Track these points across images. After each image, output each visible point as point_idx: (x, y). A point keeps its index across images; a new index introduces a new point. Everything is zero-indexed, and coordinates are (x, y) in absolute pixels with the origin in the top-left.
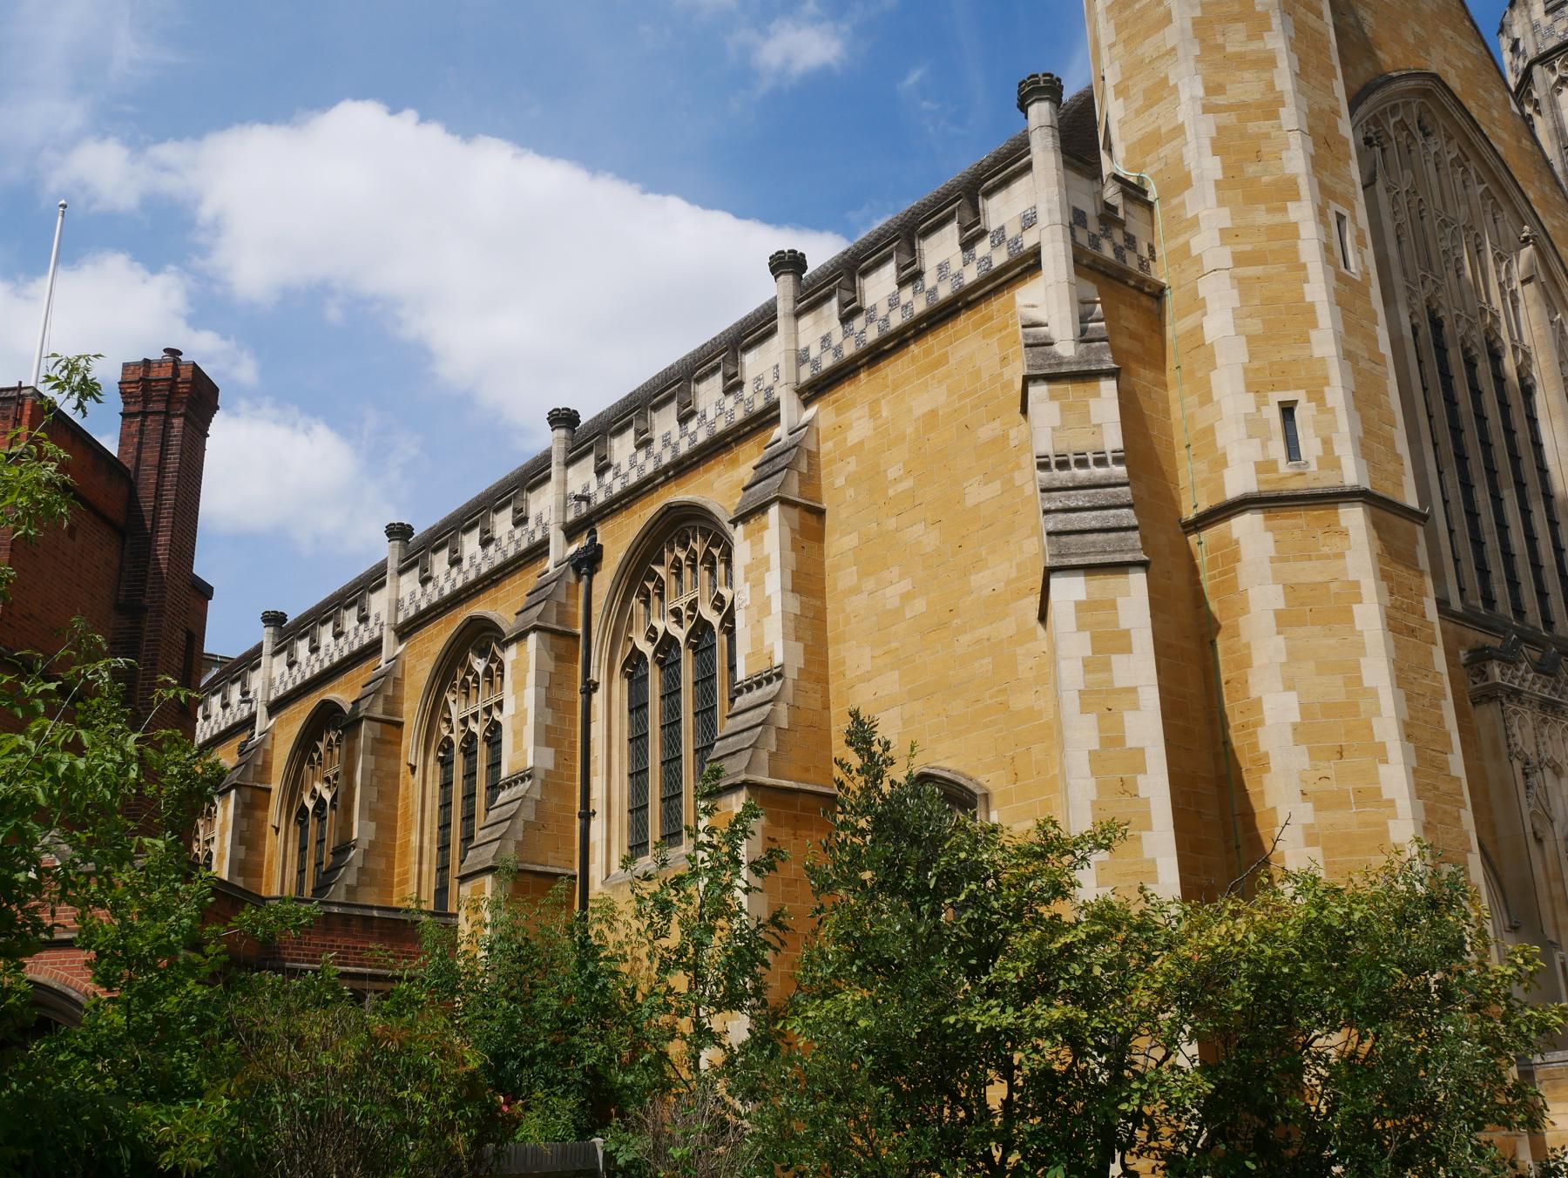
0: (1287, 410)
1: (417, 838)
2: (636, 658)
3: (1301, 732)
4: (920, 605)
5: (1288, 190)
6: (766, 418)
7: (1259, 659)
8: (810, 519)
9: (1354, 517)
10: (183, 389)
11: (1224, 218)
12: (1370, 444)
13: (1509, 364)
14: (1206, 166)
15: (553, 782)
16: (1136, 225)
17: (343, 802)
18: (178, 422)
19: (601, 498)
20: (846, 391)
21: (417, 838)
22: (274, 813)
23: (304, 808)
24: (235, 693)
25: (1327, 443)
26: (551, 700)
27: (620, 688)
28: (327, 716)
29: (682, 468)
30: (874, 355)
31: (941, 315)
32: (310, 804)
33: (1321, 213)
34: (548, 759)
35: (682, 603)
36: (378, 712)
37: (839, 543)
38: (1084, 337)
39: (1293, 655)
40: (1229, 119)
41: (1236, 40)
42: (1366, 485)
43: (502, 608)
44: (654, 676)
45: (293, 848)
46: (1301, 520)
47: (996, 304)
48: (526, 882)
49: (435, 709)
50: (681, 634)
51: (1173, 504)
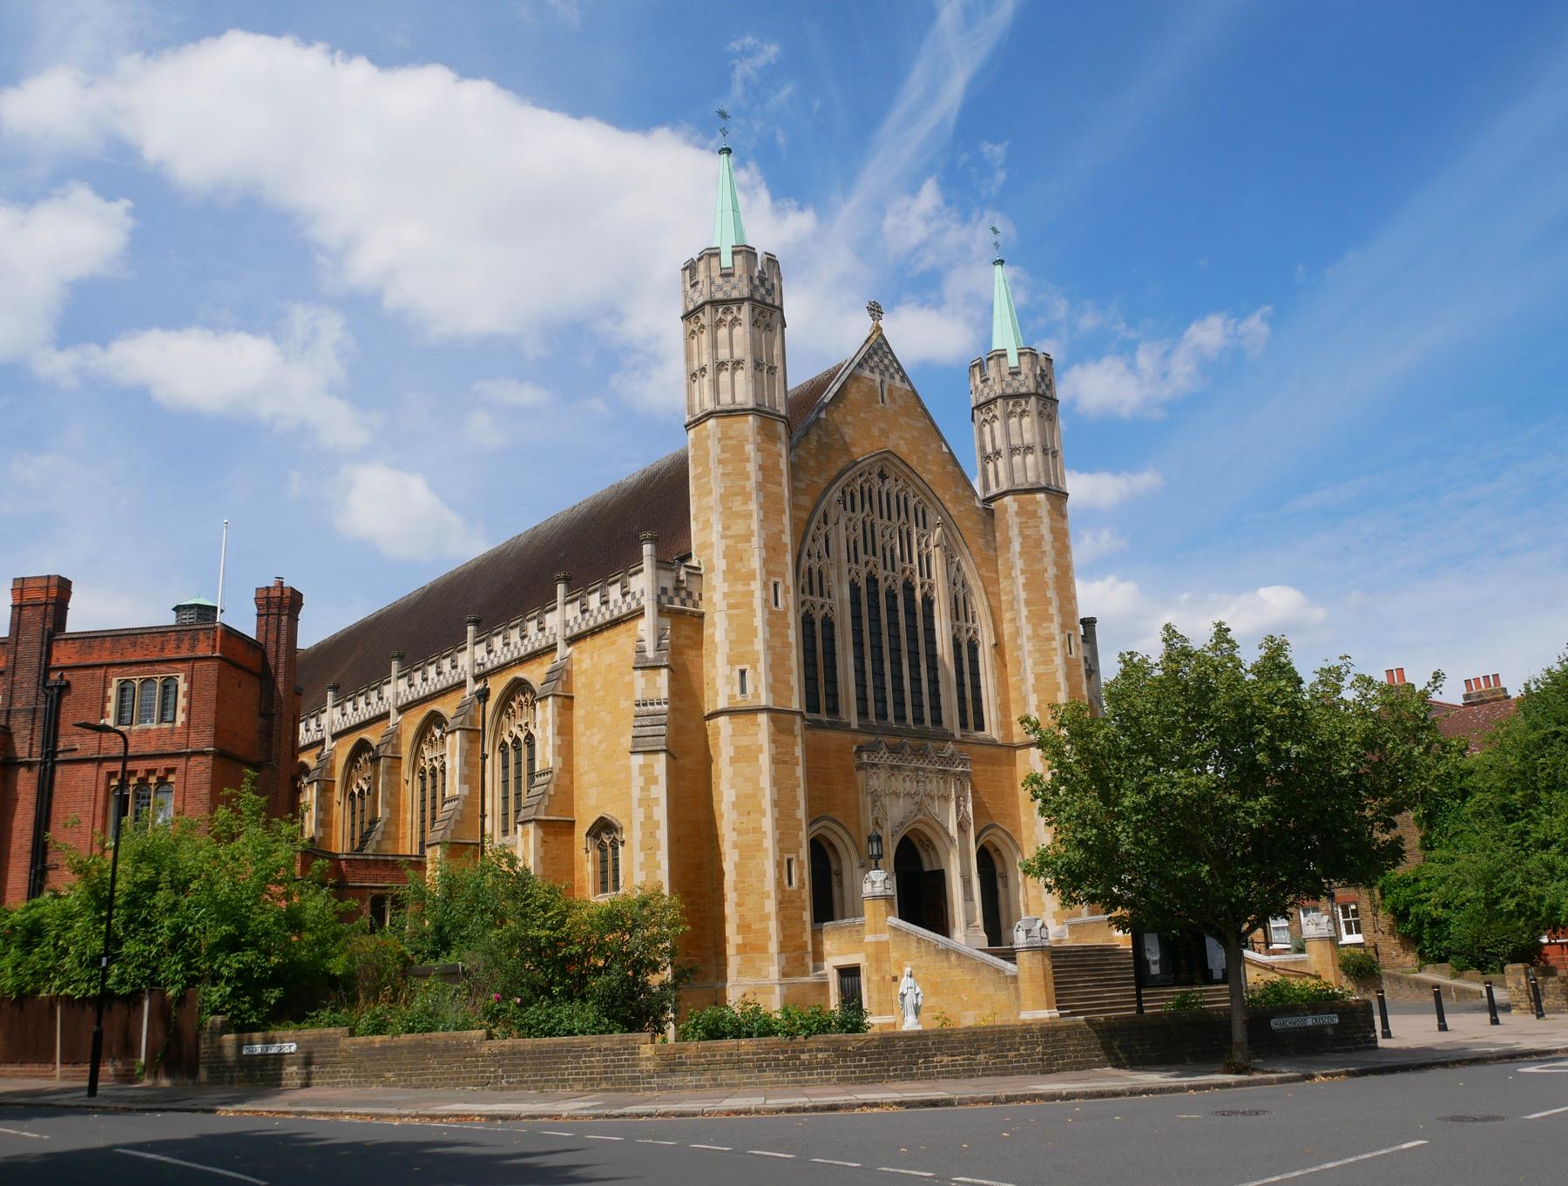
0: (743, 673)
1: (410, 815)
2: (504, 744)
4: (604, 746)
5: (751, 576)
6: (552, 648)
7: (724, 776)
9: (763, 719)
10: (286, 601)
11: (725, 588)
12: (777, 683)
14: (721, 564)
15: (467, 801)
16: (693, 587)
17: (373, 791)
18: (284, 618)
19: (489, 666)
20: (582, 644)
21: (410, 815)
23: (353, 793)
25: (756, 687)
26: (467, 761)
27: (498, 757)
28: (363, 746)
29: (522, 661)
32: (356, 791)
33: (765, 586)
34: (466, 790)
35: (522, 723)
36: (389, 753)
37: (579, 712)
38: (658, 647)
39: (735, 773)
40: (731, 542)
41: (737, 505)
42: (771, 705)
43: (447, 707)
44: (512, 754)
45: (348, 812)
46: (743, 719)
47: (633, 624)
48: (455, 849)
49: (417, 753)
50: (522, 736)
51: (700, 708)
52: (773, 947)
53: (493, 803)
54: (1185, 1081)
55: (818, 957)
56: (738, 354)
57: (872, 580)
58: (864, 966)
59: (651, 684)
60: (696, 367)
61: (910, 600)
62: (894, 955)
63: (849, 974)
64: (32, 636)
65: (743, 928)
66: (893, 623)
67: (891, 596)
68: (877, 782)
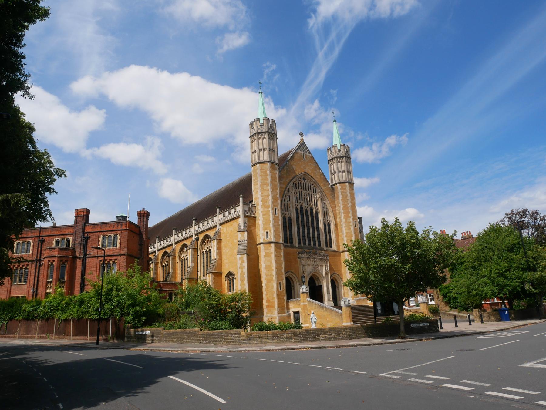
0: (267, 232)
1: (179, 271)
2: (203, 252)
3: (265, 268)
5: (269, 206)
6: (216, 227)
8: (220, 241)
9: (273, 245)
13: (314, 211)
14: (261, 203)
15: (194, 267)
16: (253, 210)
17: (169, 265)
20: (224, 225)
21: (179, 271)
22: (159, 266)
24: (153, 247)
27: (202, 256)
28: (166, 253)
29: (208, 230)
30: (227, 222)
31: (232, 219)
37: (223, 244)
38: (244, 226)
40: (263, 197)
41: (265, 187)
43: (188, 242)
44: (205, 255)
46: (267, 245)
48: (190, 280)
51: (256, 242)
52: (276, 306)
53: (200, 268)
54: (388, 341)
55: (288, 309)
56: (265, 147)
57: (302, 207)
58: (300, 311)
59: (242, 236)
60: (253, 150)
61: (312, 213)
62: (309, 308)
63: (296, 313)
64: (80, 225)
65: (268, 301)
66: (307, 219)
67: (307, 211)
68: (303, 262)
